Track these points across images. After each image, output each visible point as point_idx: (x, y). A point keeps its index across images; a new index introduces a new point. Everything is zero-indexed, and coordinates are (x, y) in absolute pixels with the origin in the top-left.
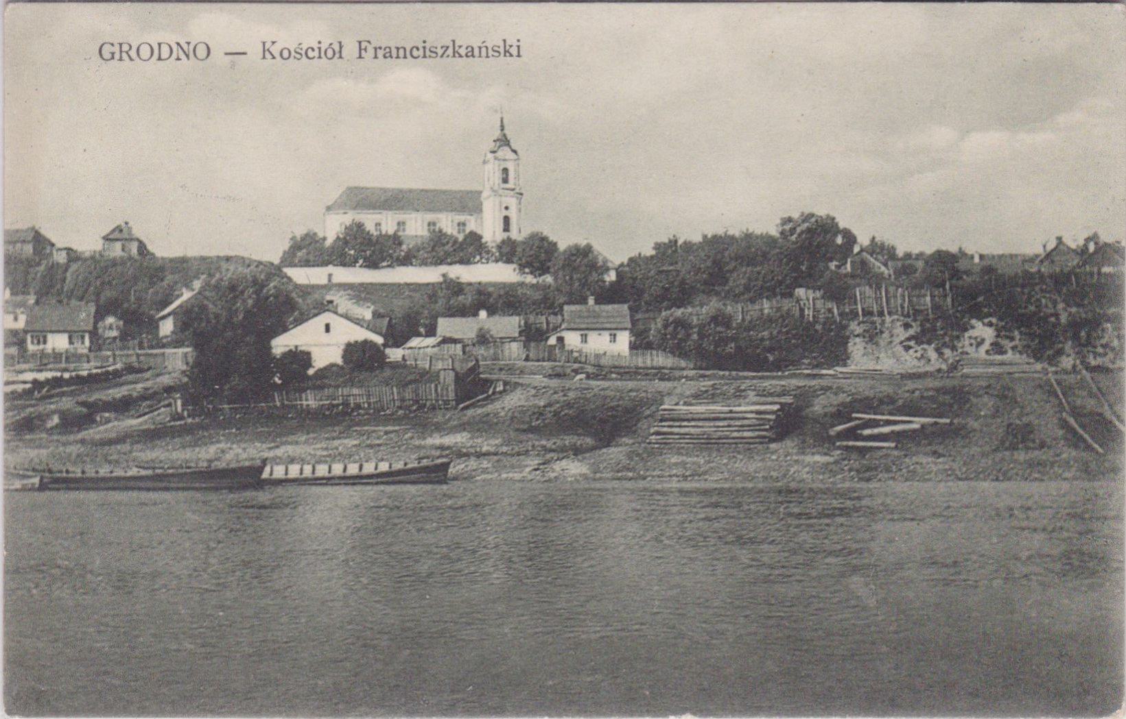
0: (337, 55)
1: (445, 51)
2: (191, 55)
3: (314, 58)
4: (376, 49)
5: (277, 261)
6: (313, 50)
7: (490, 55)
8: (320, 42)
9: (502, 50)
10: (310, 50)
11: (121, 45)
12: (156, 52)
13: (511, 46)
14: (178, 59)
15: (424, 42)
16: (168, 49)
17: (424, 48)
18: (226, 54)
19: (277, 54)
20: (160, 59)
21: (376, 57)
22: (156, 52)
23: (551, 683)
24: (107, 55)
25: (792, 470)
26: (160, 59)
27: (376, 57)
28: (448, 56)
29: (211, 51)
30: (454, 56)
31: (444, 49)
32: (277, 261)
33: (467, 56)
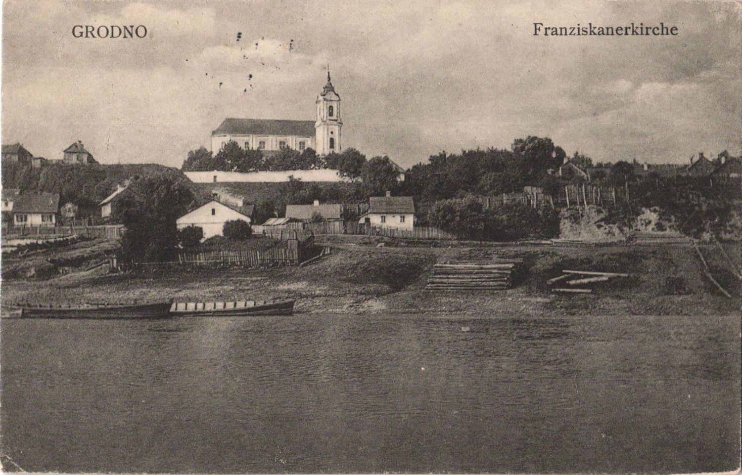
2: (123, 29)
3: (659, 34)
4: (546, 29)
7: (581, 33)
8: (642, 24)
9: (588, 30)
10: (656, 29)
11: (87, 27)
13: (595, 28)
16: (100, 33)
17: (579, 28)
18: (240, 34)
20: (112, 36)
24: (77, 33)
27: (546, 34)
28: (574, 34)
29: (147, 28)
30: (633, 34)
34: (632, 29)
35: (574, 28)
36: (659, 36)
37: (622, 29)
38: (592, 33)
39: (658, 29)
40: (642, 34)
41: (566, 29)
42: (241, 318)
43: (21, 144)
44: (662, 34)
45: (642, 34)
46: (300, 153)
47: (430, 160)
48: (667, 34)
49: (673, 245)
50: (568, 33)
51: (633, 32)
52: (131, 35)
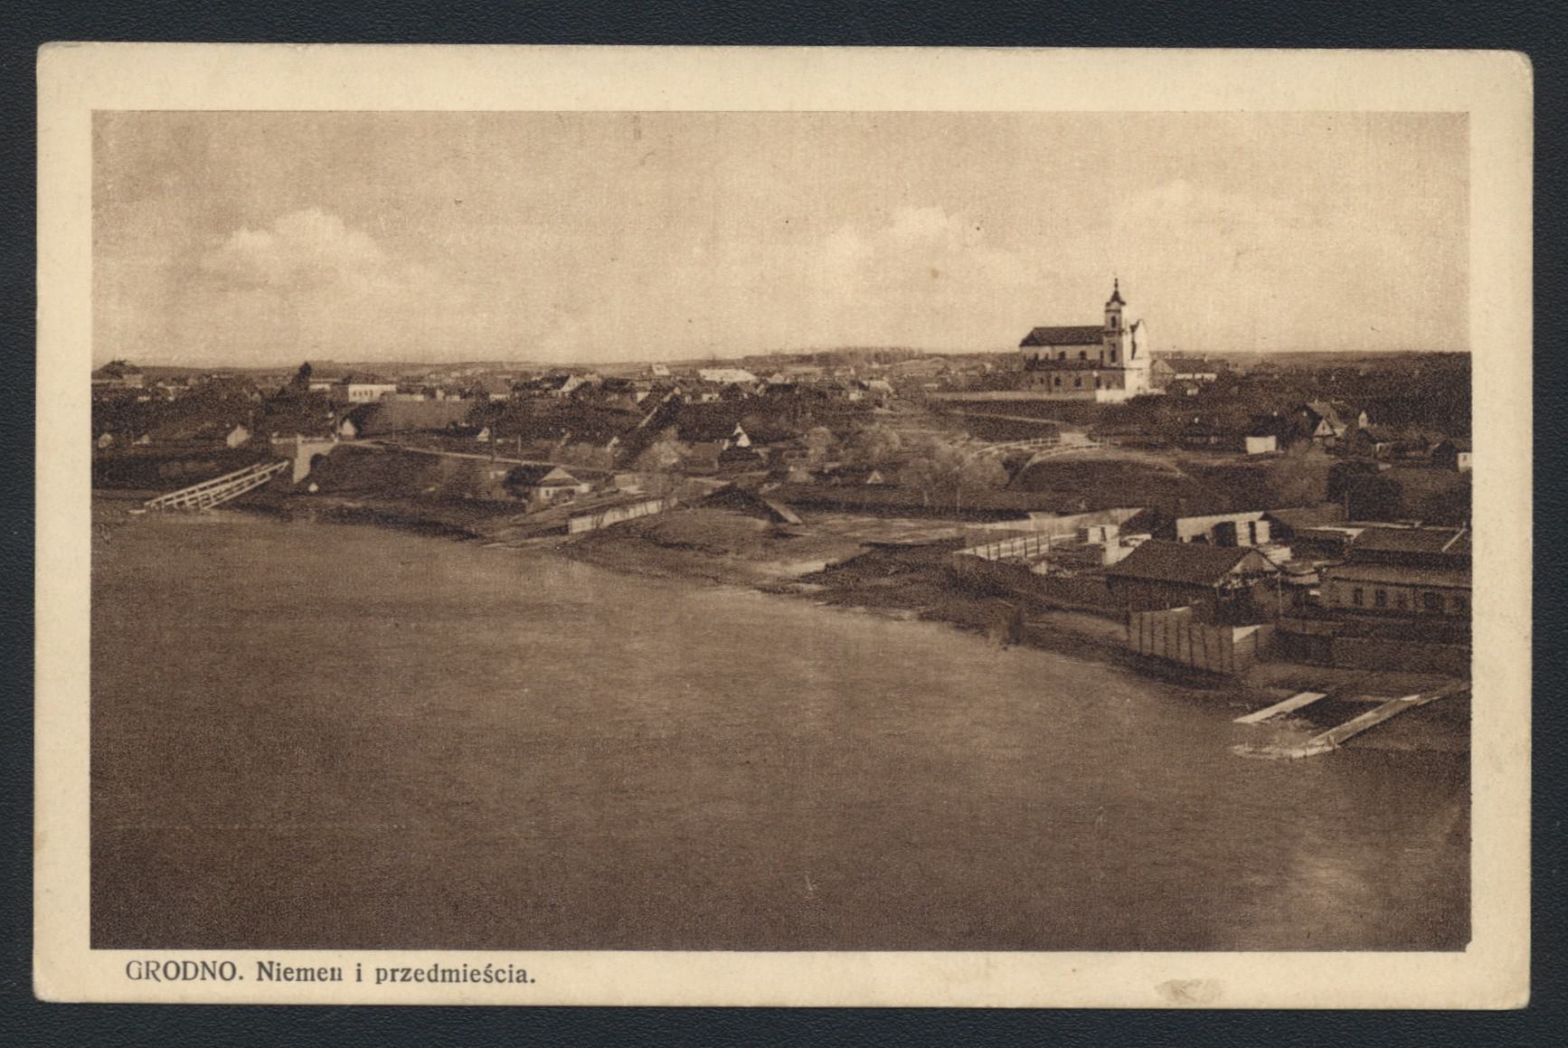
0: (181, 975)
1: (405, 976)
3: (504, 980)
6: (504, 972)
8: (465, 965)
10: (500, 973)
11: (148, 964)
14: (203, 979)
15: (511, 966)
17: (511, 972)
18: (359, 979)
23: (208, 424)
24: (134, 973)
26: (185, 978)
29: (125, 971)
31: (408, 977)
33: (518, 980)
36: (293, 982)
37: (326, 972)
39: (504, 972)
43: (1117, 540)
44: (299, 979)
46: (1320, 400)
49: (1338, 563)
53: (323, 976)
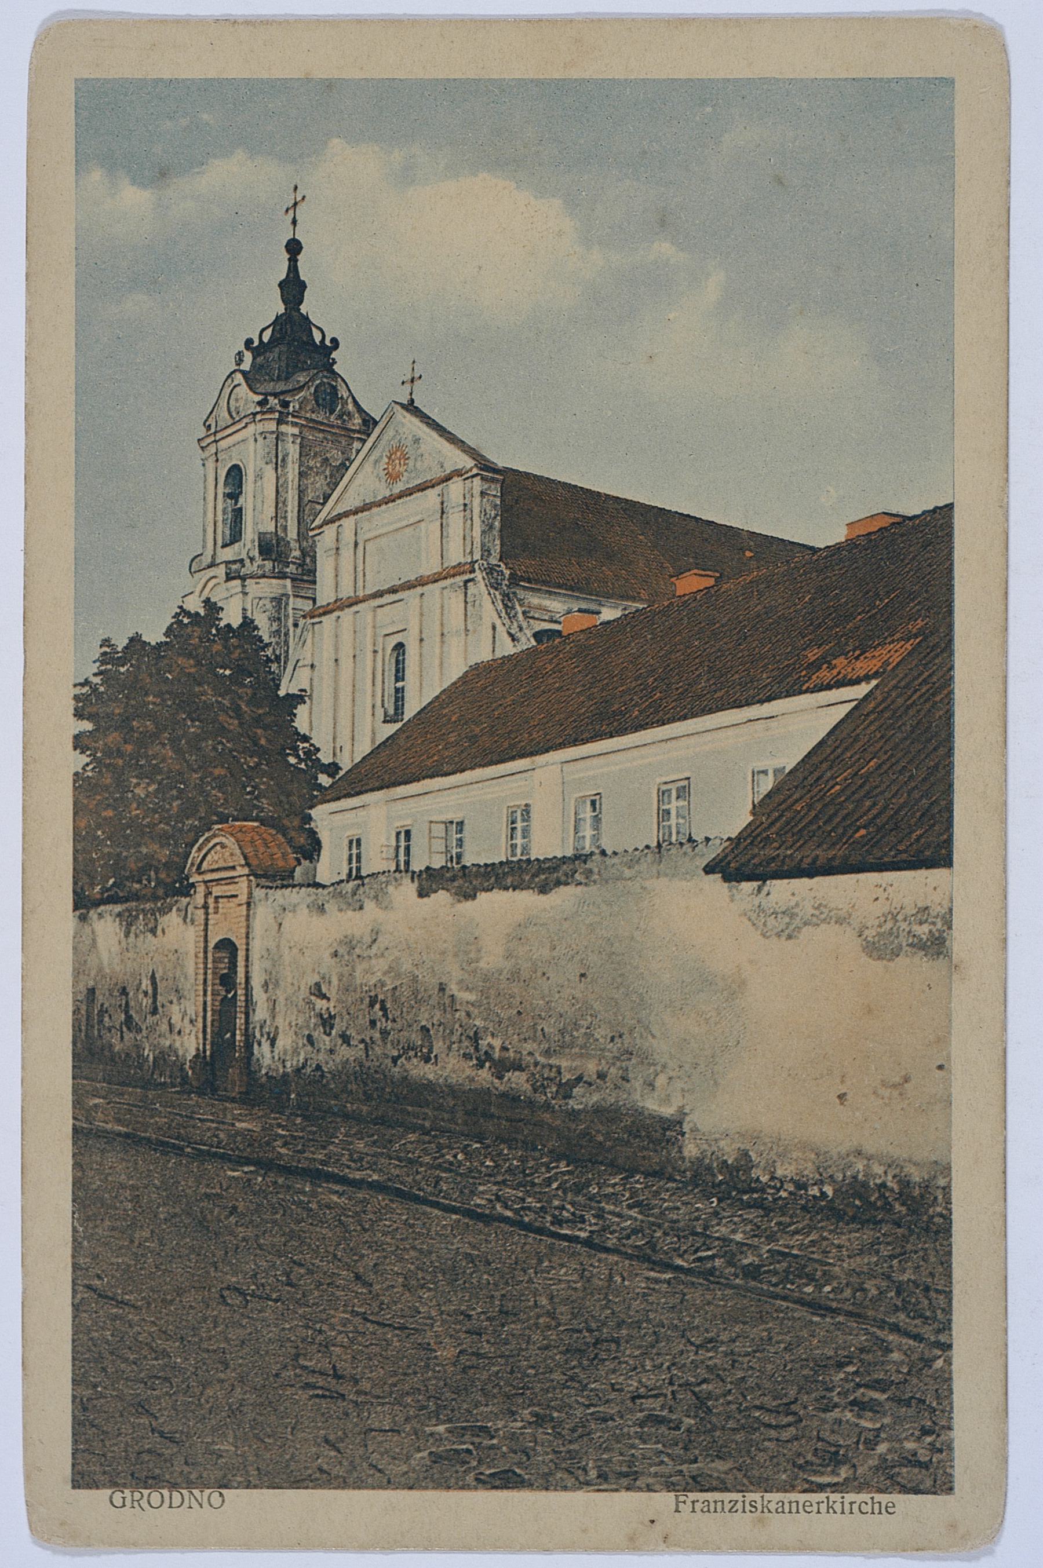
4: (693, 1502)
5: (281, 309)
12: (801, 1507)
13: (834, 1502)
14: (190, 1507)
17: (744, 1502)
19: (773, 1510)
20: (170, 1507)
21: (693, 1511)
22: (801, 1507)
25: (730, 646)
26: (170, 1507)
27: (693, 1511)
30: (828, 1512)
32: (281, 309)
34: (825, 1504)
35: (737, 1501)
38: (765, 1510)
40: (843, 1513)
41: (723, 1502)
42: (360, 476)
45: (843, 1513)
47: (79, 714)
48: (880, 1513)
50: (726, 1510)
51: (828, 1508)
52: (201, 1506)
53: (808, 1509)
